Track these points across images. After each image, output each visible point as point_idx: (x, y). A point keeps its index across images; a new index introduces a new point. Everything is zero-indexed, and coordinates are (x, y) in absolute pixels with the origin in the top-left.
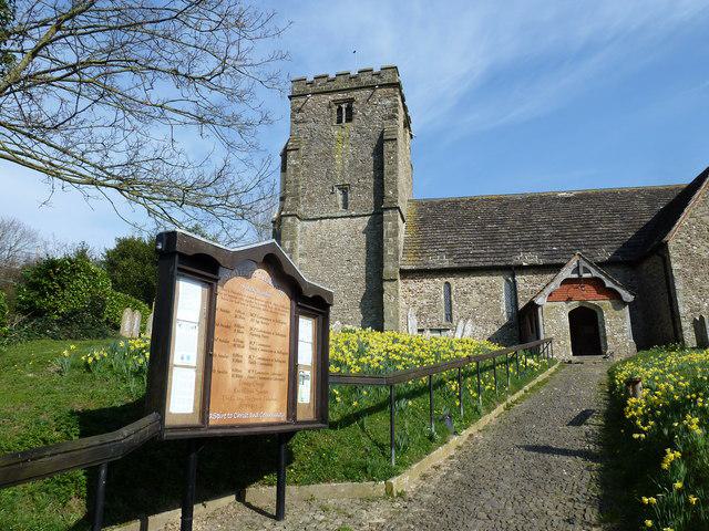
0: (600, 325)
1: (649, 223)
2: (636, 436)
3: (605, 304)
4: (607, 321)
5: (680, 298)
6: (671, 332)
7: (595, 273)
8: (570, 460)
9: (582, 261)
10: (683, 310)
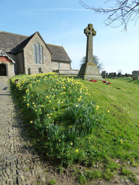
0: (7, 69)
1: (20, 44)
2: (19, 89)
3: (8, 63)
4: (9, 67)
5: (25, 63)
6: (23, 71)
7: (6, 55)
8: (5, 96)
9: (3, 51)
10: (26, 66)
